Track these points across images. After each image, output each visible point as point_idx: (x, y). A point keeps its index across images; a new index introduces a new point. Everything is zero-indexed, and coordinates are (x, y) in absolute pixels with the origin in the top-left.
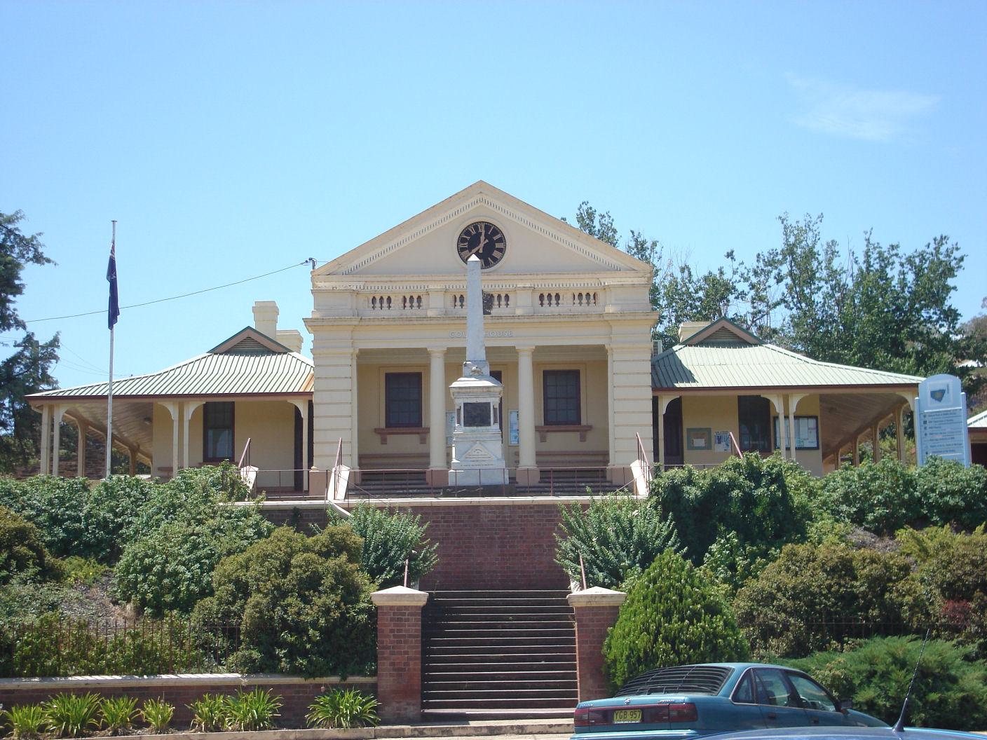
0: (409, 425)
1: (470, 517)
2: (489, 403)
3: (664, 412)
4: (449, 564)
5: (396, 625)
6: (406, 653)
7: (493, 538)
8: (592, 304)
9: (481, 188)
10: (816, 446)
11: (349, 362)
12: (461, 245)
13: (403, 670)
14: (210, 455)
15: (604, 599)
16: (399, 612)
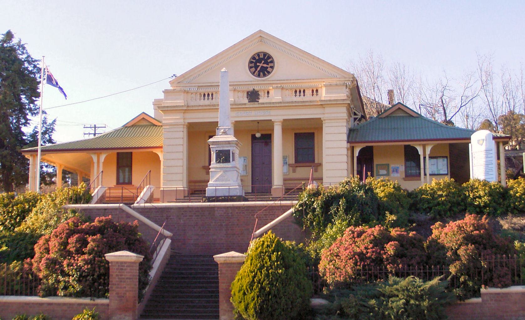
0: (308, 161)
1: (209, 214)
2: (229, 150)
3: (357, 155)
4: (198, 239)
5: (120, 272)
6: (125, 287)
7: (221, 225)
8: (298, 96)
9: (261, 36)
10: (446, 173)
11: (182, 129)
12: (251, 65)
13: (123, 297)
14: (121, 181)
15: (234, 259)
16: (121, 265)
